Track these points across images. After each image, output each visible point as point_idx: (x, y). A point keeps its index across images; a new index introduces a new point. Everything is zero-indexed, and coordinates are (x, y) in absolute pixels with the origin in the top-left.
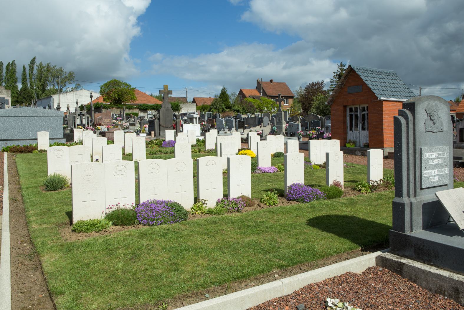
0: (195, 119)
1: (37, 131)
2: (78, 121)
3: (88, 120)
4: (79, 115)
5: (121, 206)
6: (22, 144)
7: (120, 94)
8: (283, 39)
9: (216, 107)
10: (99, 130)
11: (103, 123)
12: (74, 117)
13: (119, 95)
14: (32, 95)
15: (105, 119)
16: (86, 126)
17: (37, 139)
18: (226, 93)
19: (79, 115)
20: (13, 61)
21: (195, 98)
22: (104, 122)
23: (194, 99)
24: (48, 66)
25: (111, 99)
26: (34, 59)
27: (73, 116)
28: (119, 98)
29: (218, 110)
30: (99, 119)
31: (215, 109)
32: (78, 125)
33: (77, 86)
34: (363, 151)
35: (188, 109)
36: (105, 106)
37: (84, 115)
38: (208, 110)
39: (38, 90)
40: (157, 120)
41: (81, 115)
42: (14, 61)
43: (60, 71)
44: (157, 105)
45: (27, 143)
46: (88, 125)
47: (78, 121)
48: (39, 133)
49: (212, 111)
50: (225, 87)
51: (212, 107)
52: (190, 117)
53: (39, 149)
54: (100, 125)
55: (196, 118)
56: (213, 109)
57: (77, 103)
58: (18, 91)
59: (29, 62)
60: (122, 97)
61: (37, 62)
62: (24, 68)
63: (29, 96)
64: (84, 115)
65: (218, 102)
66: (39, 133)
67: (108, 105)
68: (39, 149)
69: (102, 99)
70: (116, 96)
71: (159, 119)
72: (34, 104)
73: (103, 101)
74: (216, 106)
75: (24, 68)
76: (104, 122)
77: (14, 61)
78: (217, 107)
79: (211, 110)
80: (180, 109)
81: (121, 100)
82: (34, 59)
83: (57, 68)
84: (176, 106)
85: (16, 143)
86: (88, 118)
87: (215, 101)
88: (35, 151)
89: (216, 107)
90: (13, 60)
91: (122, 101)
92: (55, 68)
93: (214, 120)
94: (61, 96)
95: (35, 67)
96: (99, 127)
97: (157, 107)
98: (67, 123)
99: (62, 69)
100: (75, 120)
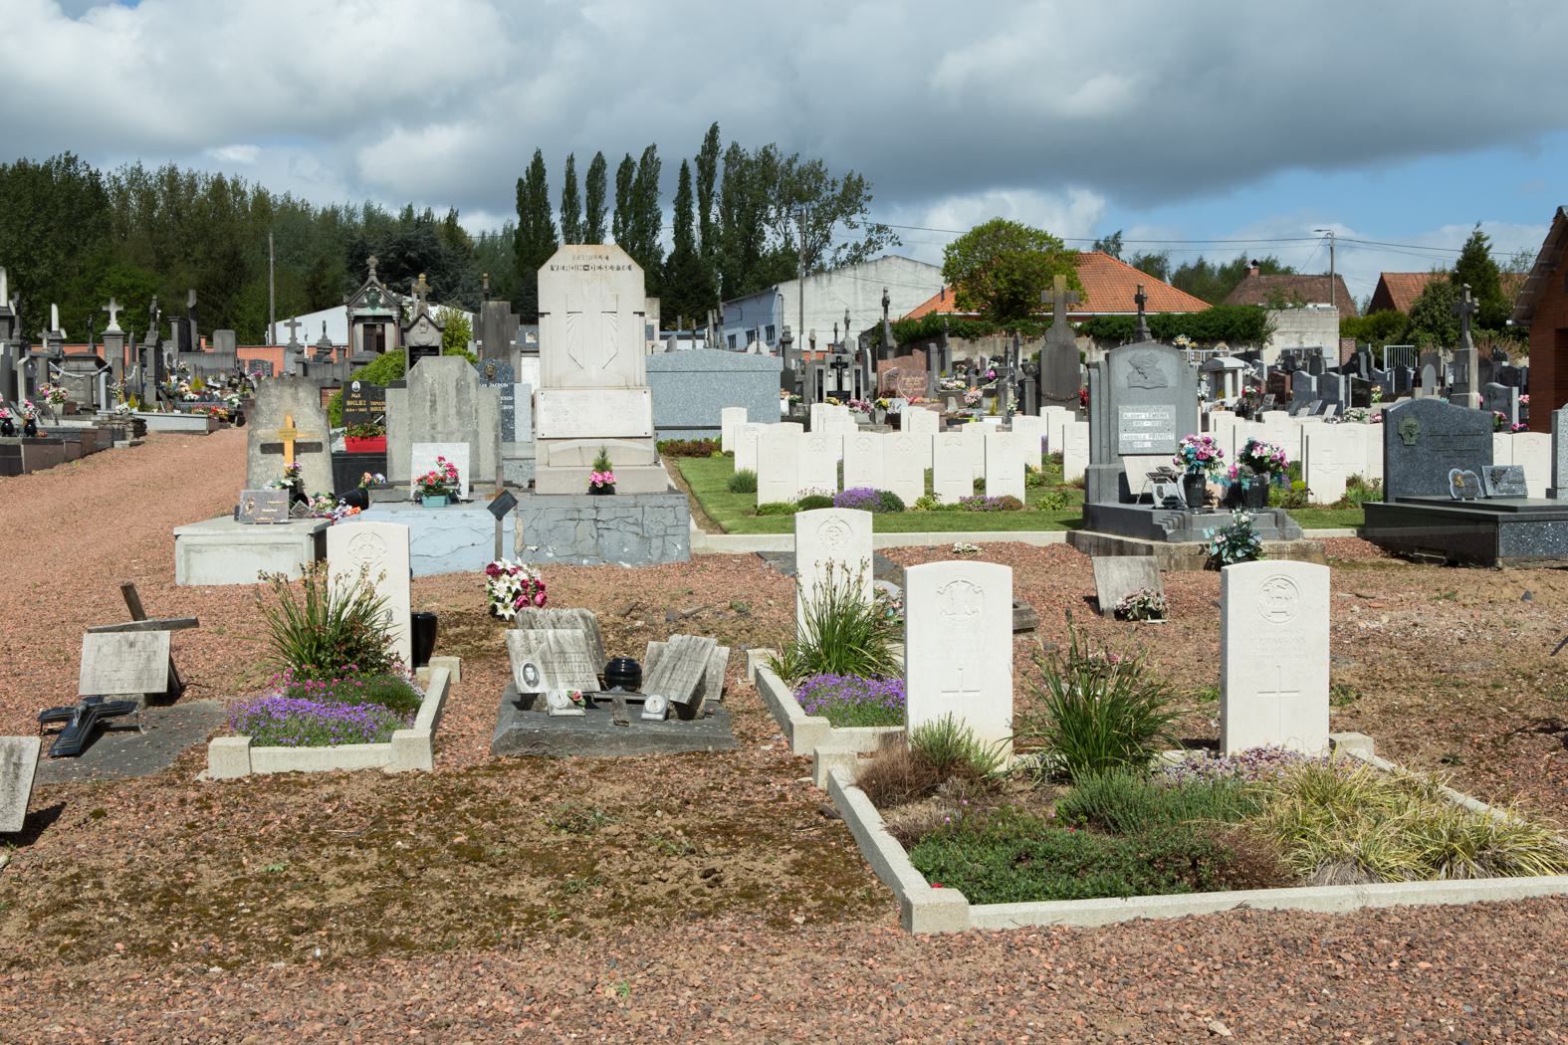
0: (1229, 377)
1: (749, 163)
2: (830, 384)
3: (858, 382)
4: (833, 366)
5: (817, 493)
6: (688, 437)
7: (1017, 276)
8: (188, 567)
9: (1430, 322)
10: (885, 408)
11: (900, 390)
12: (820, 372)
13: (1014, 283)
14: (707, 281)
15: (907, 375)
16: (853, 399)
17: (719, 428)
18: (1485, 256)
19: (833, 366)
20: (650, 150)
21: (1386, 278)
22: (904, 386)
23: (1382, 280)
24: (767, 156)
25: (987, 298)
26: (714, 130)
27: (818, 367)
28: (1015, 294)
29: (1443, 333)
30: (892, 377)
31: (1429, 328)
32: (829, 394)
33: (874, 237)
34: (465, 347)
35: (1302, 333)
36: (961, 325)
37: (846, 365)
38: (1398, 335)
39: (728, 260)
40: (1030, 379)
41: (839, 365)
42: (654, 147)
43: (816, 172)
44: (1169, 317)
45: (699, 436)
46: (858, 397)
47: (830, 384)
48: (724, 411)
49: (1413, 341)
50: (1486, 229)
51: (1414, 322)
52: (1217, 368)
53: (724, 450)
54: (892, 394)
55: (1234, 372)
56: (1416, 332)
57: (886, 303)
58: (661, 266)
59: (693, 149)
60: (1027, 287)
61: (724, 145)
62: (685, 170)
63: (697, 286)
64: (846, 365)
65: (1441, 300)
66: (724, 411)
67: (970, 323)
68: (724, 450)
69: (951, 300)
70: (1003, 284)
71: (1038, 379)
72: (715, 325)
73: (956, 306)
74: (1433, 317)
75: (685, 170)
76: (904, 386)
77: (654, 147)
78: (1435, 322)
79: (1410, 336)
80: (1268, 333)
81: (1022, 302)
82: (714, 130)
83: (802, 162)
84: (1249, 322)
85: (677, 436)
86: (857, 372)
87: (1431, 293)
88: (716, 454)
89: (1430, 322)
90: (650, 144)
91: (1030, 306)
92: (795, 167)
93: (1288, 378)
94: (810, 285)
95: (720, 164)
96: (886, 401)
97: (1164, 327)
98: (802, 389)
99: (823, 169)
100: (821, 381)
